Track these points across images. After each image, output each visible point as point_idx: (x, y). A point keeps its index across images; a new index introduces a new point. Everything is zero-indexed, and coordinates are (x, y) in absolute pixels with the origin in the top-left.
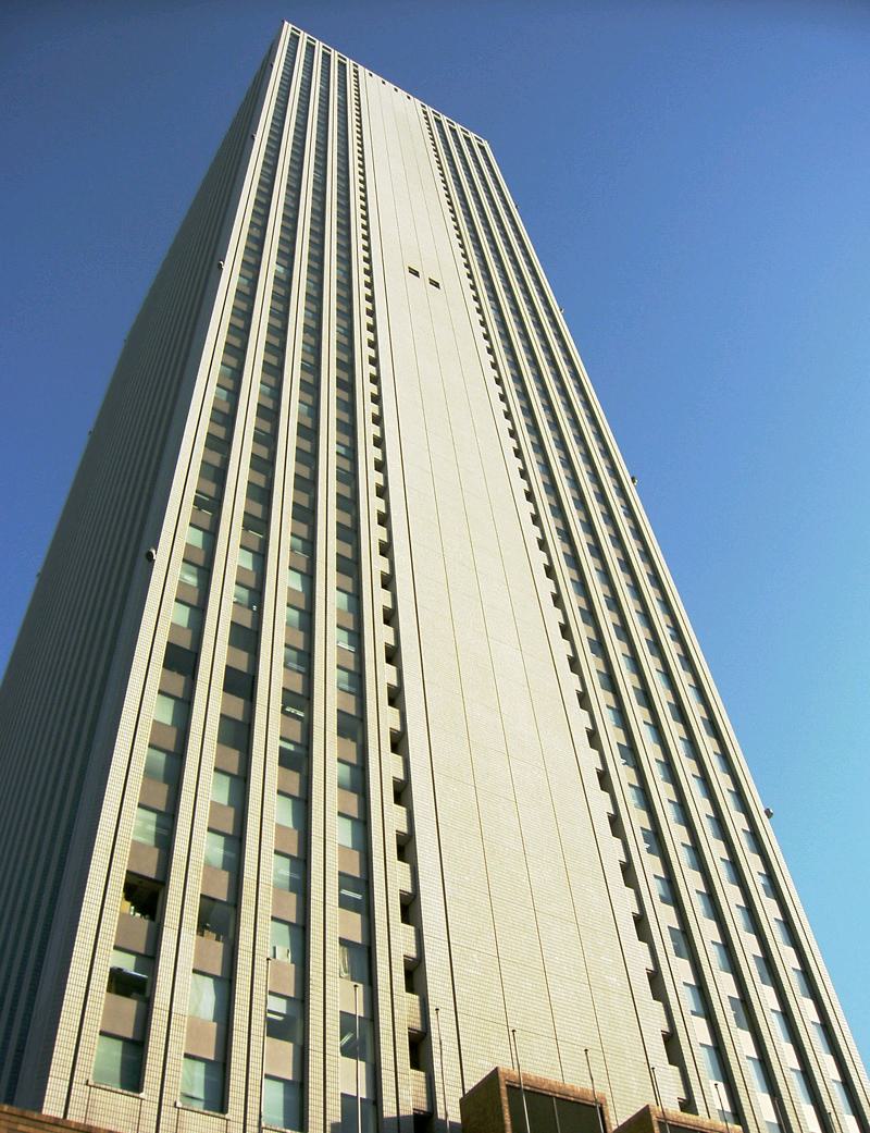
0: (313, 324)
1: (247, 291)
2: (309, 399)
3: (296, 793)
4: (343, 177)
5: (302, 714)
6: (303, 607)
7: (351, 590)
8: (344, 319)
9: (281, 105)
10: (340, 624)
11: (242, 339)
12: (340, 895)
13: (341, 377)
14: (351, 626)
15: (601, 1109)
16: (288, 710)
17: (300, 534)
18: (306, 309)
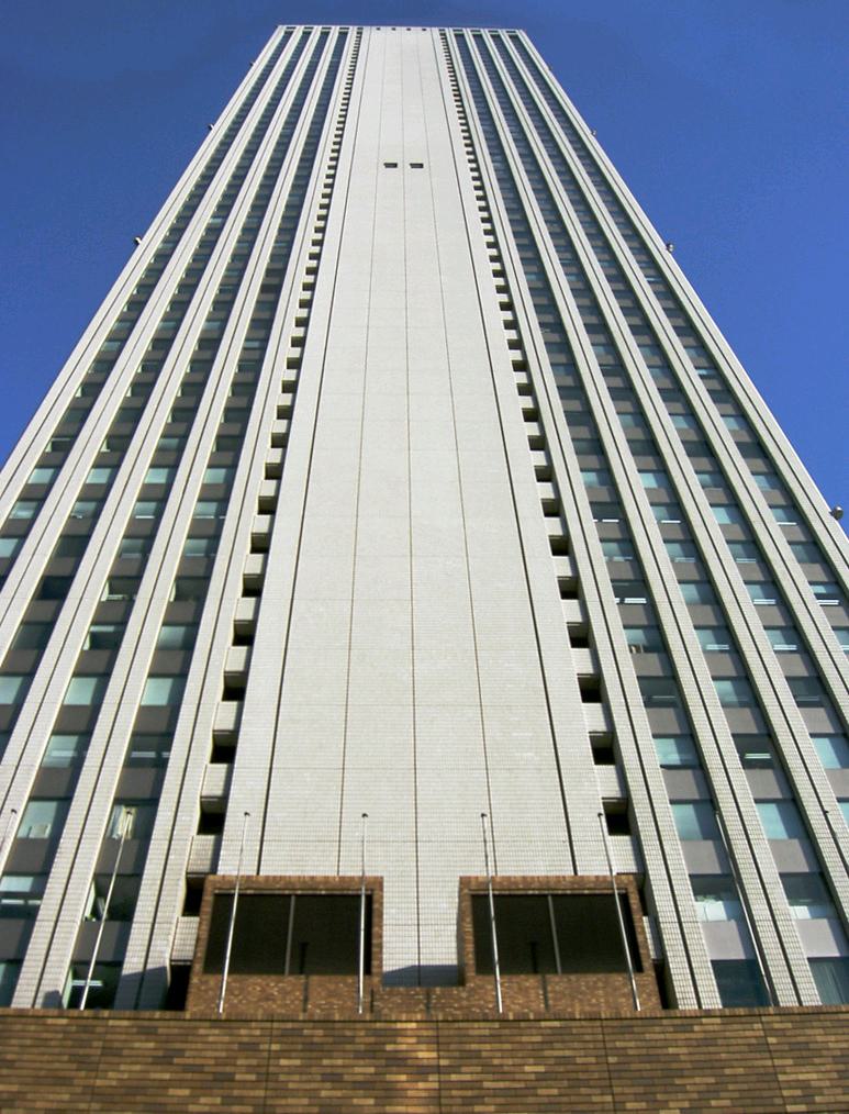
0: (594, 320)
1: (540, 285)
2: (628, 406)
3: (713, 622)
4: (567, 178)
5: (766, 756)
6: (667, 500)
7: (683, 412)
8: (624, 298)
9: (494, 143)
10: (767, 624)
11: (580, 399)
12: (738, 565)
13: (633, 323)
14: (780, 622)
15: (369, 899)
16: (750, 756)
17: (673, 537)
18: (593, 344)
